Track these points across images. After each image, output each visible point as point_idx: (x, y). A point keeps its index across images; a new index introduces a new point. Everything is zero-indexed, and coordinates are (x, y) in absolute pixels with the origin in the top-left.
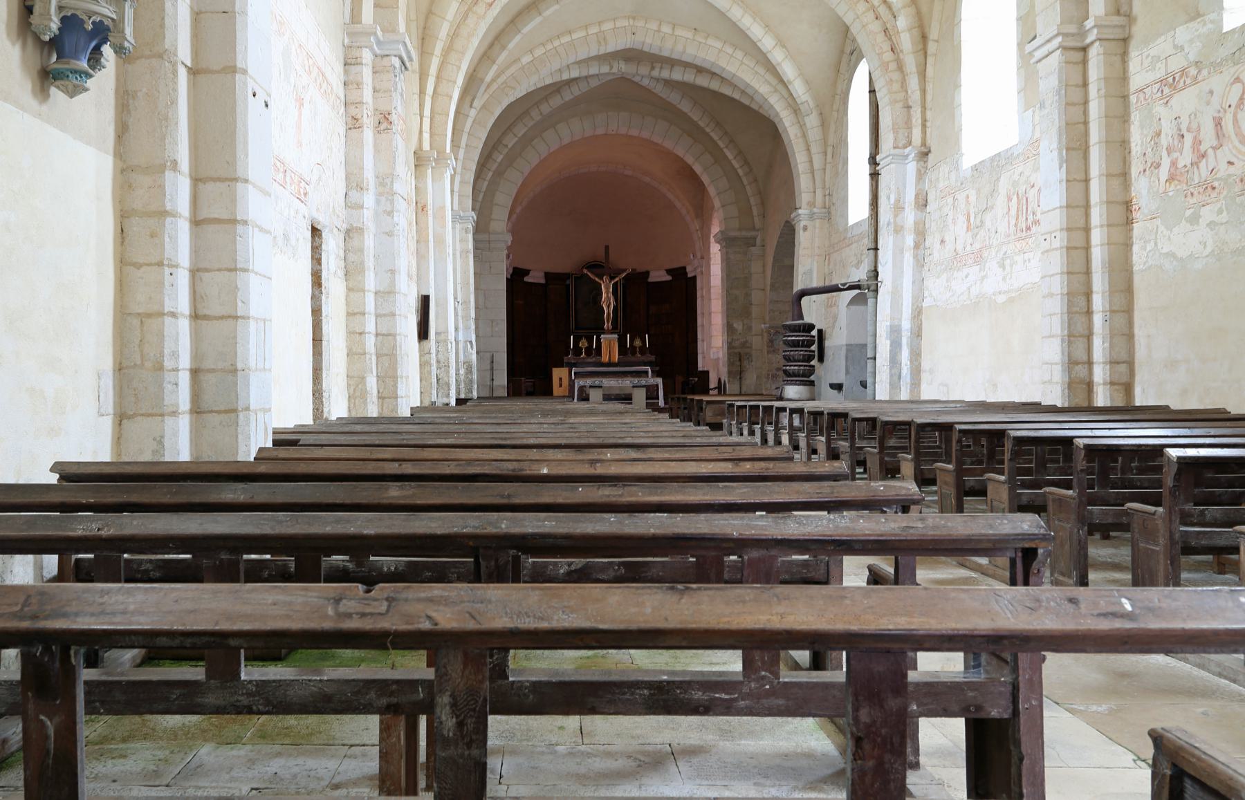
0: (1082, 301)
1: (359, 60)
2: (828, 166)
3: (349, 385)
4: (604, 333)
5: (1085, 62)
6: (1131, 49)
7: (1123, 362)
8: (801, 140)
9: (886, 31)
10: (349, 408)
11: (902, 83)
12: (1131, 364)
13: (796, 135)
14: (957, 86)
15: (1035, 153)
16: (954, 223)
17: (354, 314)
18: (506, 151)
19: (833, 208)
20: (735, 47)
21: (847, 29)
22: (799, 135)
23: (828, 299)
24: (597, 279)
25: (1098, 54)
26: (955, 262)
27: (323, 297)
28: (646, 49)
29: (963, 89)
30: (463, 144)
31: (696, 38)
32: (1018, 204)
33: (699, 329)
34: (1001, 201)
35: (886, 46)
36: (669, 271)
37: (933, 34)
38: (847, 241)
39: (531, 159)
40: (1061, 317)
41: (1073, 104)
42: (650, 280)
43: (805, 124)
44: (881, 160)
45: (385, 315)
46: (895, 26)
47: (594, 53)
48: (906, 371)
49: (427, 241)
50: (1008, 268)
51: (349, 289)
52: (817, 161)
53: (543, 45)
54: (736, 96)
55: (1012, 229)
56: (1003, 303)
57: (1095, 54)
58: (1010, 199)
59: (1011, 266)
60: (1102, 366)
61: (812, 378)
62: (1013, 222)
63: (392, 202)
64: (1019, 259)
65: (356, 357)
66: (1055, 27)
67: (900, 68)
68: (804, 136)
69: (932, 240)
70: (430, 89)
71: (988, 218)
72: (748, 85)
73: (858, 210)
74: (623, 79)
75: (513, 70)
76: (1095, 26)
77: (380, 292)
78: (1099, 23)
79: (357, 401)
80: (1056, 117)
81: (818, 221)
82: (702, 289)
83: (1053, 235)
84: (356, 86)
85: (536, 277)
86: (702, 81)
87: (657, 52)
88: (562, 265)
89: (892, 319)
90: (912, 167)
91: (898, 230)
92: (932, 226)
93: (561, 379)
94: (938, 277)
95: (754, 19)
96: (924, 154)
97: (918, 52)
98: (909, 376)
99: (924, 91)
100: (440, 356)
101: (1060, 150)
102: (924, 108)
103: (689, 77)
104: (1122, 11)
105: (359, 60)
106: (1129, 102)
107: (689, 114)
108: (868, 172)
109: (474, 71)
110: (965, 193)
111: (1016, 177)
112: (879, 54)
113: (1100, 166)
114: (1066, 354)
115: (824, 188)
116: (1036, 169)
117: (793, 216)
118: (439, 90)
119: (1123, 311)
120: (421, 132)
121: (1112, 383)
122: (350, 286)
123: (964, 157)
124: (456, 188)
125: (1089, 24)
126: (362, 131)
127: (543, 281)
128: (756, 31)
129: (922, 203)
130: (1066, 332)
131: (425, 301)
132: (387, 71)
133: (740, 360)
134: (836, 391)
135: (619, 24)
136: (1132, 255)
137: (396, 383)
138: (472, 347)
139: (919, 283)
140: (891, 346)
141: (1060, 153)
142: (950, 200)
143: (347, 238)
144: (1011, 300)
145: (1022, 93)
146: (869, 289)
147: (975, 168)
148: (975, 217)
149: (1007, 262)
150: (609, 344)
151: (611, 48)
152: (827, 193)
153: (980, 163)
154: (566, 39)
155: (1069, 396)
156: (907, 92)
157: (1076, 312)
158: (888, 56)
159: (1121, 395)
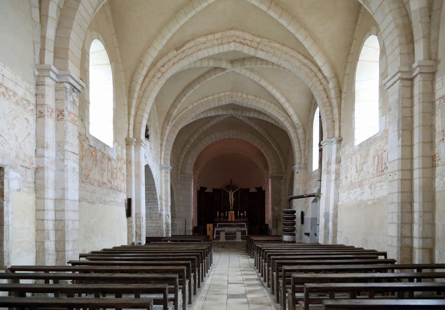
0: (408, 206)
1: (43, 83)
2: (306, 149)
3: (36, 246)
4: (230, 210)
5: (412, 86)
6: (436, 78)
7: (429, 238)
8: (296, 139)
9: (325, 89)
10: (36, 257)
11: (331, 111)
12: (433, 239)
13: (294, 137)
14: (353, 110)
15: (386, 135)
16: (351, 169)
17: (40, 210)
18: (191, 144)
19: (308, 165)
20: (271, 102)
21: (313, 96)
22: (296, 137)
23: (305, 200)
24: (228, 191)
25: (419, 81)
26: (351, 186)
27: (5, 203)
28: (237, 104)
29: (356, 112)
30: (165, 139)
31: (256, 99)
32: (378, 160)
33: (266, 209)
34: (370, 159)
35: (325, 96)
36: (256, 189)
37: (344, 90)
38: (312, 177)
39: (201, 147)
40: (398, 214)
41: (406, 107)
42: (250, 191)
43: (298, 133)
44: (323, 144)
45: (60, 211)
46: (328, 87)
47: (217, 105)
48: (331, 231)
49: (131, 176)
50: (373, 189)
51: (37, 198)
52: (302, 148)
53: (197, 101)
54: (273, 122)
55: (375, 171)
56: (371, 204)
57: (418, 82)
58: (374, 158)
59: (375, 188)
60: (418, 239)
61: (294, 232)
62: (376, 168)
63: (64, 155)
64: (378, 185)
65: (40, 232)
66: (397, 68)
67: (331, 105)
68: (298, 137)
69: (342, 177)
70: (133, 112)
71: (365, 167)
72: (271, 114)
73: (315, 166)
74: (232, 117)
75: (185, 111)
76: (418, 66)
77: (57, 199)
78: (420, 64)
79: (40, 253)
80: (397, 114)
81: (302, 169)
82: (267, 195)
83: (394, 173)
84: (42, 96)
85: (209, 190)
86: (261, 117)
87: (241, 105)
88: (218, 186)
89: (326, 209)
90: (334, 146)
91: (329, 173)
92: (342, 171)
93: (210, 228)
94: (344, 192)
95: (277, 91)
96: (340, 141)
97: (338, 97)
98: (332, 233)
99: (340, 114)
100: (137, 223)
101: (398, 130)
102: (340, 121)
103: (256, 116)
104: (432, 58)
105: (43, 83)
106: (435, 105)
107: (258, 130)
108: (318, 149)
109: (169, 111)
110: (356, 156)
111: (377, 148)
112: (321, 99)
113: (419, 138)
114: (400, 232)
115: (305, 157)
116: (387, 143)
117: (293, 168)
118: (138, 113)
119: (430, 212)
120: (129, 130)
121: (423, 248)
122: (38, 196)
123: (355, 141)
124: (163, 156)
125: (415, 65)
126: (44, 119)
127: (212, 192)
128: (278, 95)
129: (339, 161)
130: (400, 222)
131: (129, 201)
132: (62, 90)
133: (277, 221)
134: (307, 236)
135: (226, 93)
136: (435, 183)
137: (65, 244)
138: (169, 217)
139: (337, 195)
140: (325, 221)
141: (399, 132)
142: (349, 159)
143: (36, 172)
144: (374, 204)
145: (381, 109)
146: (318, 197)
147: (360, 145)
148: (360, 167)
149: (373, 186)
150: (231, 214)
151: (223, 103)
152: (306, 159)
153: (362, 143)
154: (206, 99)
155: (401, 254)
156: (333, 115)
157: (405, 212)
158: (326, 100)
159: (428, 254)
